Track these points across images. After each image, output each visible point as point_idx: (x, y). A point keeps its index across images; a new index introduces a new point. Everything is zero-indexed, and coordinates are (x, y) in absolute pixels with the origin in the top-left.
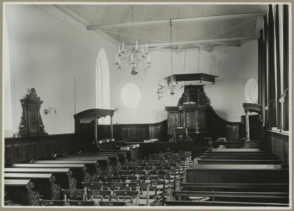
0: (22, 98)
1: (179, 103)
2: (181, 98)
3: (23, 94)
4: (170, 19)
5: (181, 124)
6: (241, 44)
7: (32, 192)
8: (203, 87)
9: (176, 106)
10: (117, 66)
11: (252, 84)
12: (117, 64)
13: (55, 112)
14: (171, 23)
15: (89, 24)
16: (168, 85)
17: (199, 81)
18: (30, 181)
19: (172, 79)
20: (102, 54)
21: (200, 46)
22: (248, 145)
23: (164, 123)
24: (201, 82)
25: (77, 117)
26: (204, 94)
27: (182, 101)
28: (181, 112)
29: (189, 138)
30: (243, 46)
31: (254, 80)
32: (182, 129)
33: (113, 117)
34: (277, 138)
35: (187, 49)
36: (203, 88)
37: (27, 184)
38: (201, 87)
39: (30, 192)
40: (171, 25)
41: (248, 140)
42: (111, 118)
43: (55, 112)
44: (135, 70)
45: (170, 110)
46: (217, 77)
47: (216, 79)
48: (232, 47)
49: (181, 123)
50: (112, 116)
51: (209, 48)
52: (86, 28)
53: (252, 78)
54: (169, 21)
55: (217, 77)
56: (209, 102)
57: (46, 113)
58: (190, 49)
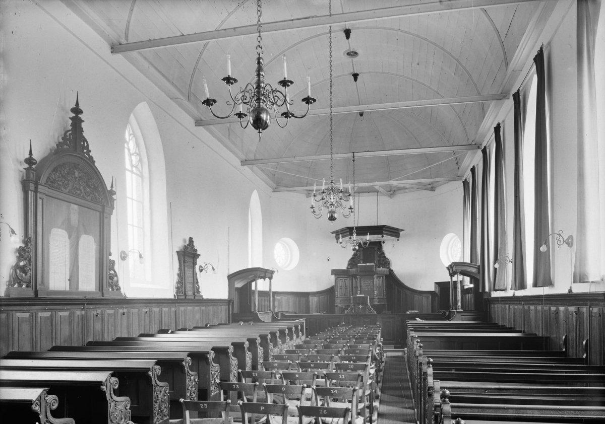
0: (178, 250)
1: (348, 265)
2: (352, 258)
3: (179, 245)
4: (354, 153)
5: (352, 293)
6: (435, 188)
7: (158, 382)
8: (382, 244)
9: (345, 268)
10: (312, 210)
11: (451, 240)
12: (312, 208)
13: (213, 268)
14: (354, 157)
15: (244, 157)
16: (336, 241)
17: (380, 236)
18: (113, 375)
19: (355, 231)
20: (255, 198)
21: (381, 190)
22: (459, 316)
23: (331, 291)
24: (383, 237)
25: (231, 278)
26: (383, 253)
27: (353, 262)
28: (354, 276)
29: (371, 309)
30: (438, 191)
31: (454, 235)
32: (363, 297)
33: (272, 280)
34: (507, 304)
35: (360, 194)
36: (381, 245)
37: (37, 399)
38: (378, 245)
39: (188, 372)
40: (354, 160)
41: (460, 310)
42: (270, 282)
43: (213, 268)
44: (334, 215)
45: (336, 272)
46: (403, 230)
47: (401, 233)
48: (424, 191)
49: (352, 291)
50: (270, 278)
51: (391, 193)
52: (240, 163)
53: (448, 233)
54: (351, 155)
55: (403, 230)
56: (389, 264)
57: (201, 271)
58: (365, 194)
